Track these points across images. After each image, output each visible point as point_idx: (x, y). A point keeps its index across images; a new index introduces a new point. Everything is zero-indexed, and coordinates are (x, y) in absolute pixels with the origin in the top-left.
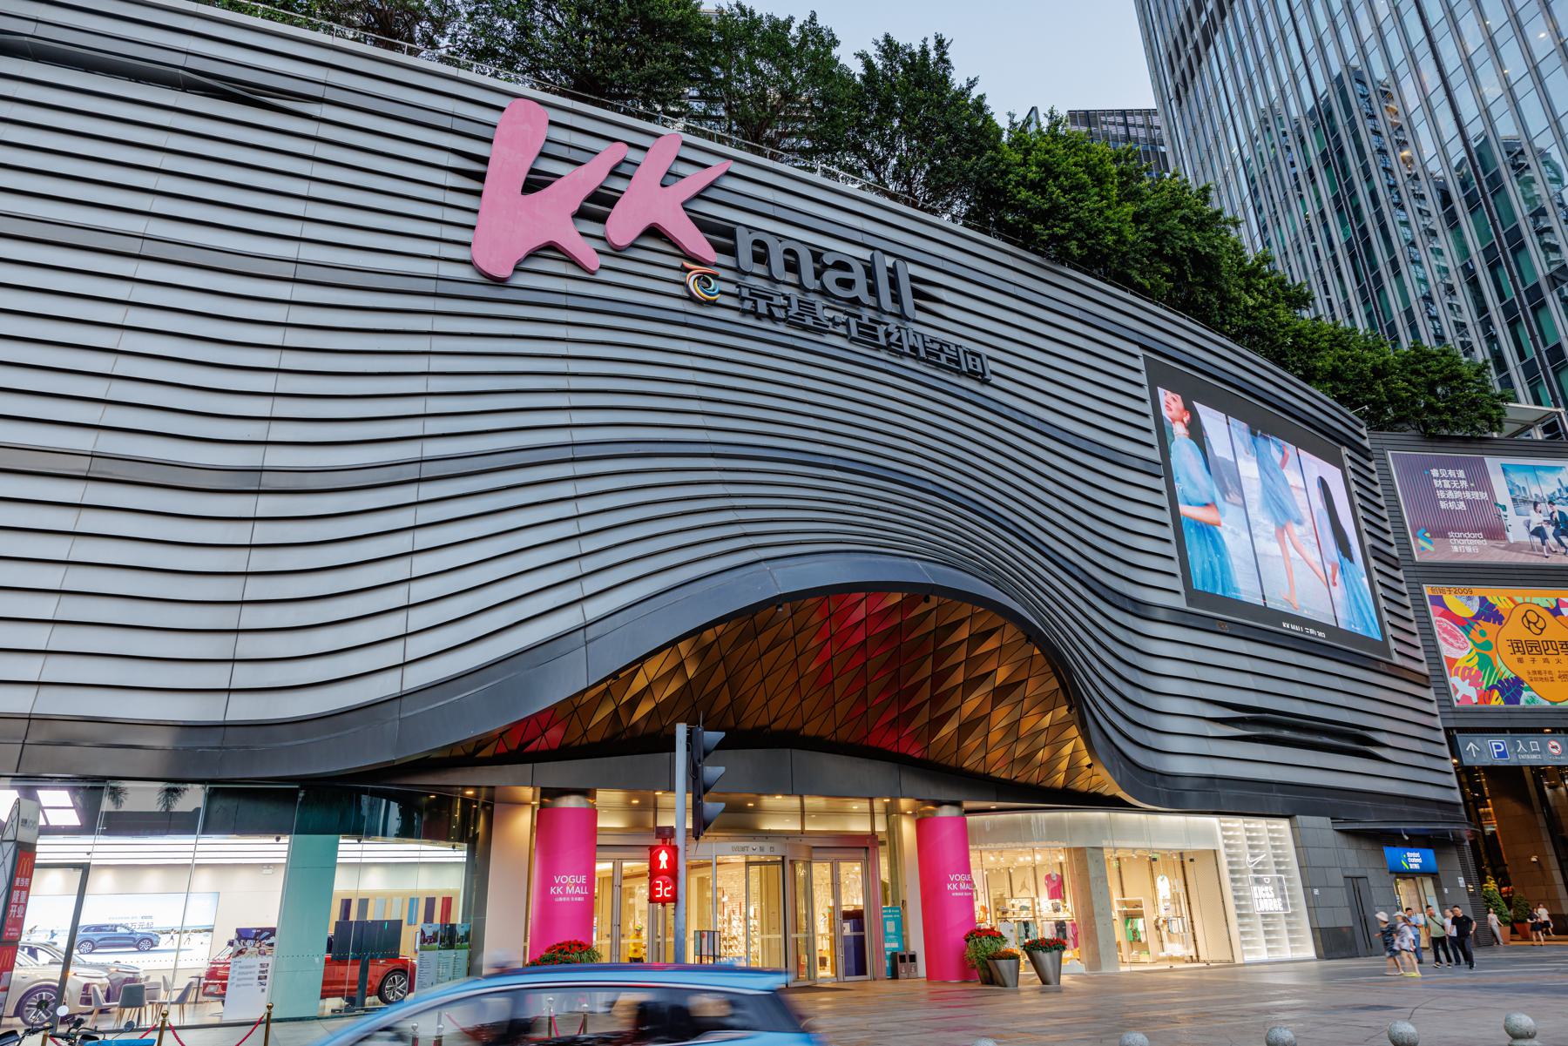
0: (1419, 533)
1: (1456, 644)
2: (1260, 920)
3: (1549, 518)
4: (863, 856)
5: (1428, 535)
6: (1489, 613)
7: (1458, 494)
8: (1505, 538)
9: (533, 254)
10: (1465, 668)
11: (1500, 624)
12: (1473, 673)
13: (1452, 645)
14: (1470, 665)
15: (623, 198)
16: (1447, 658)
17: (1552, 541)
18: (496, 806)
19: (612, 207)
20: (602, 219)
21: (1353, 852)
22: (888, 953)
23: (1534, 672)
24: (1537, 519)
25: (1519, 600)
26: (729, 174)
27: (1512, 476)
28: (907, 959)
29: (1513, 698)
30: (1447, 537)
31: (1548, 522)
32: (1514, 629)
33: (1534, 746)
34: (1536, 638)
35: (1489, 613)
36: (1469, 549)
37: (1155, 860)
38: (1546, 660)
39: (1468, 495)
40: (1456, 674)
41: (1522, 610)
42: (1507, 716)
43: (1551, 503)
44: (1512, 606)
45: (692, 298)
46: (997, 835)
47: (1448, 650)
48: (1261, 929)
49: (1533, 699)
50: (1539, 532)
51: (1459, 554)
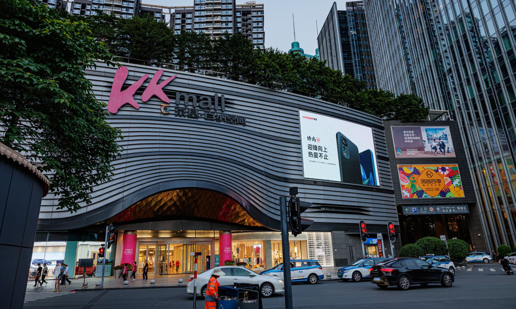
0: (398, 150)
6: (416, 172)
7: (411, 138)
8: (424, 150)
9: (123, 106)
13: (404, 181)
14: (408, 187)
15: (147, 88)
17: (438, 150)
18: (118, 234)
19: (143, 91)
20: (141, 94)
21: (351, 240)
24: (434, 144)
25: (426, 168)
26: (176, 78)
30: (406, 151)
31: (438, 145)
33: (425, 209)
34: (429, 179)
35: (416, 172)
36: (412, 154)
38: (432, 185)
39: (414, 138)
40: (404, 190)
41: (426, 171)
43: (440, 139)
45: (162, 113)
46: (237, 238)
49: (426, 196)
50: (435, 148)
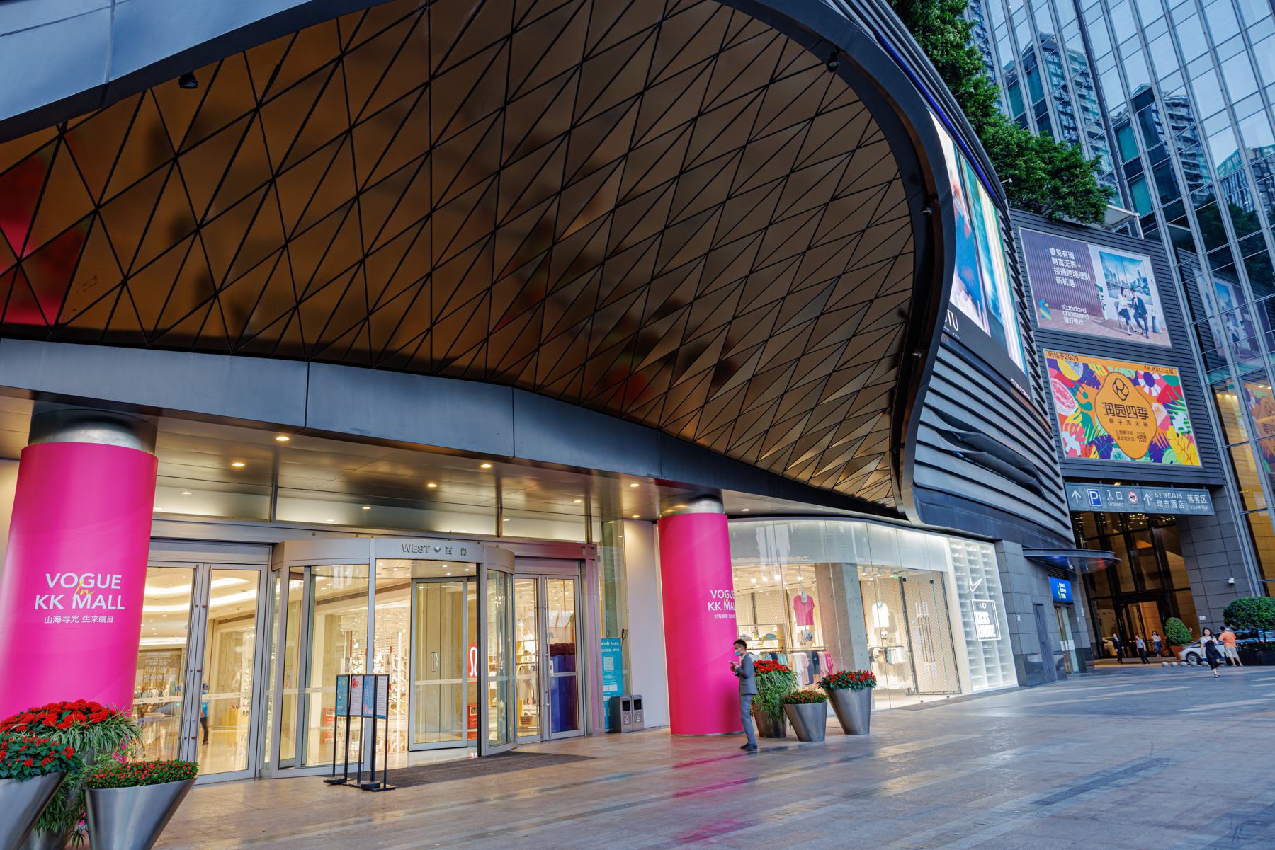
1: (1067, 404)
2: (981, 647)
3: (1131, 303)
4: (577, 571)
5: (1047, 305)
7: (1069, 273)
8: (1102, 315)
10: (1073, 424)
11: (1098, 388)
12: (1078, 429)
13: (1063, 403)
14: (1076, 422)
16: (1060, 415)
17: (1133, 322)
22: (606, 699)
23: (1121, 431)
25: (1111, 369)
27: (1107, 263)
28: (632, 705)
29: (1105, 454)
30: (1060, 309)
32: (1107, 394)
35: (1089, 378)
36: (1076, 322)
37: (904, 579)
38: (1129, 422)
40: (1066, 430)
42: (1101, 468)
43: (1132, 289)
44: (1106, 374)
47: (1061, 407)
48: (983, 656)
50: (1124, 313)
51: (1069, 325)
